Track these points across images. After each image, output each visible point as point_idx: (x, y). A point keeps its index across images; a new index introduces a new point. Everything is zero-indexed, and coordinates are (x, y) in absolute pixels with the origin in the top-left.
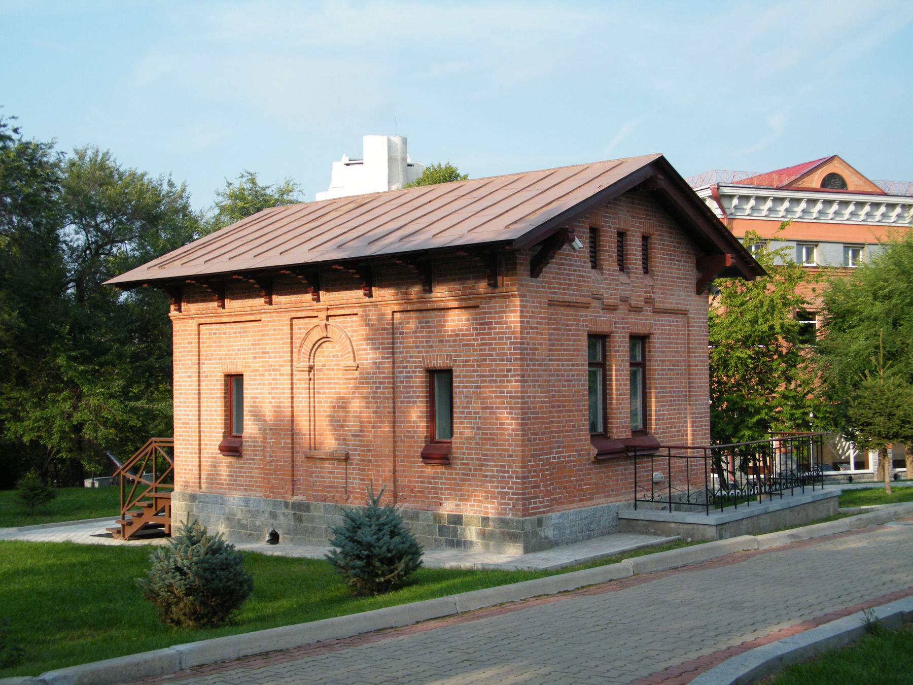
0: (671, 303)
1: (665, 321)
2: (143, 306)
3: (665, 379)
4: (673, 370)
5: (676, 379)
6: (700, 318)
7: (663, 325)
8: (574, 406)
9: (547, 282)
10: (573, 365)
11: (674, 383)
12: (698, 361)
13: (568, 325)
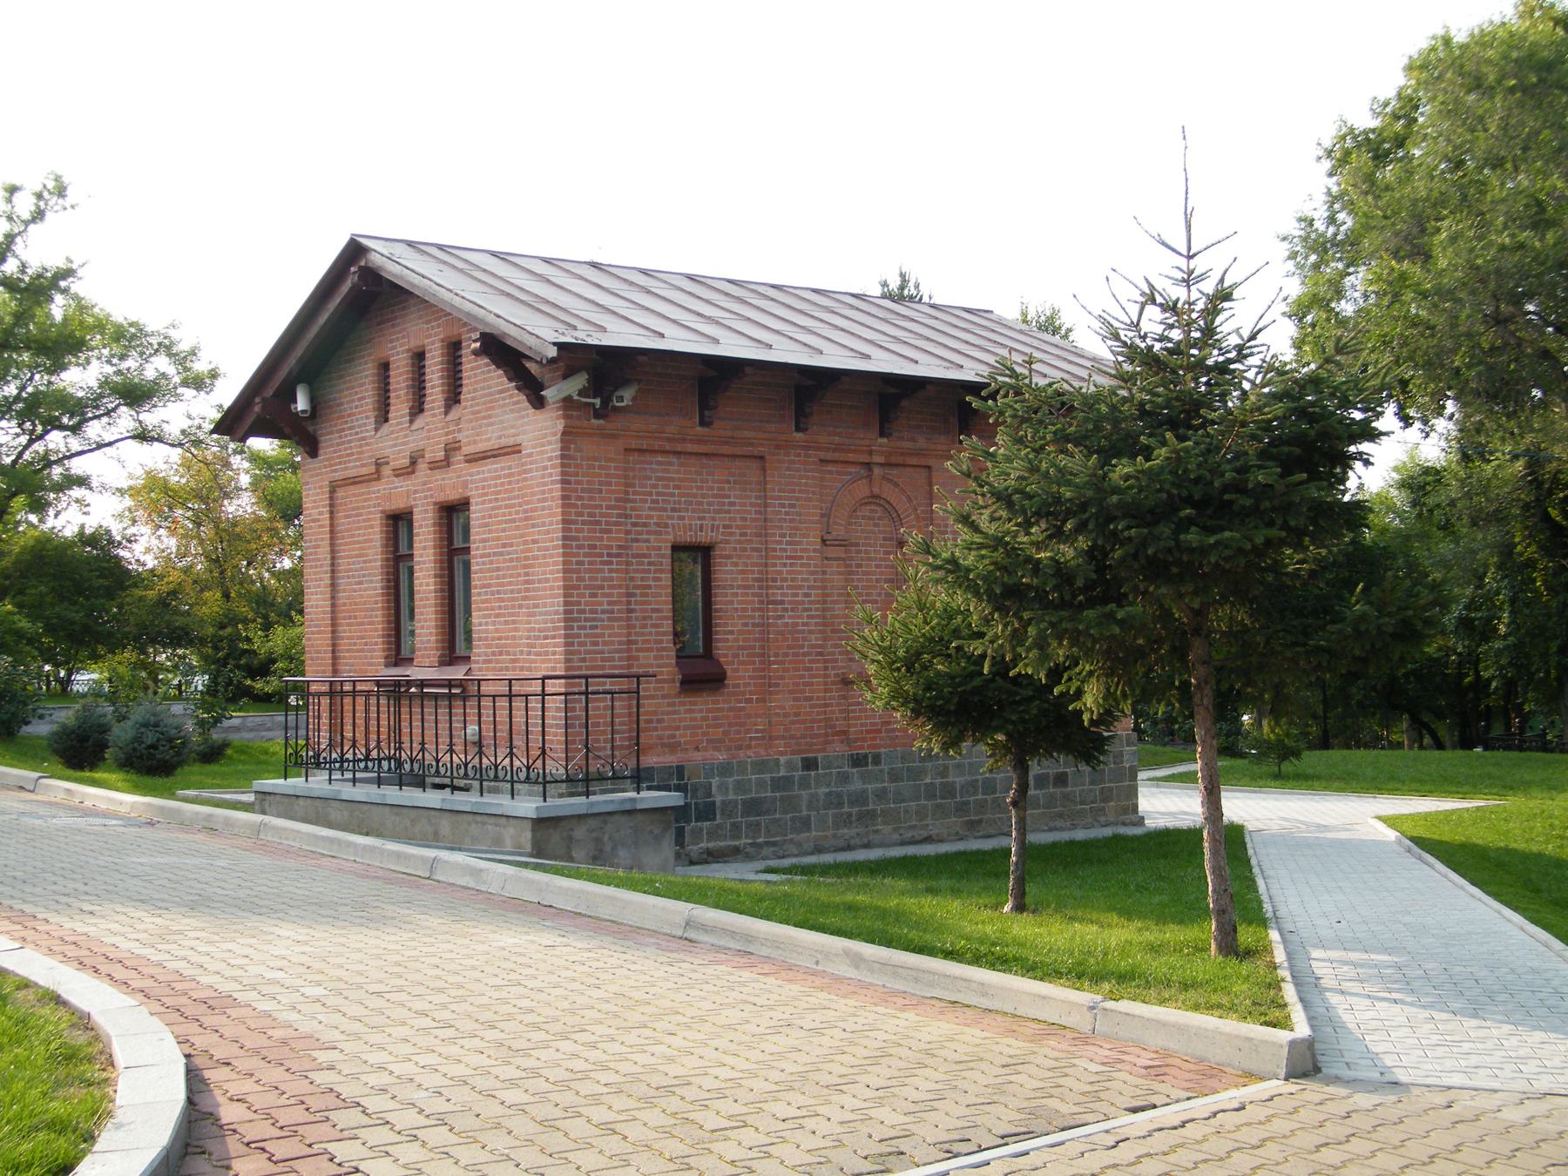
0: (489, 439)
1: (489, 471)
2: (1529, 295)
3: (490, 570)
4: (501, 554)
5: (508, 568)
6: (542, 452)
7: (484, 480)
8: (366, 617)
9: (328, 460)
10: (365, 562)
11: (504, 576)
12: (539, 533)
13: (358, 508)
